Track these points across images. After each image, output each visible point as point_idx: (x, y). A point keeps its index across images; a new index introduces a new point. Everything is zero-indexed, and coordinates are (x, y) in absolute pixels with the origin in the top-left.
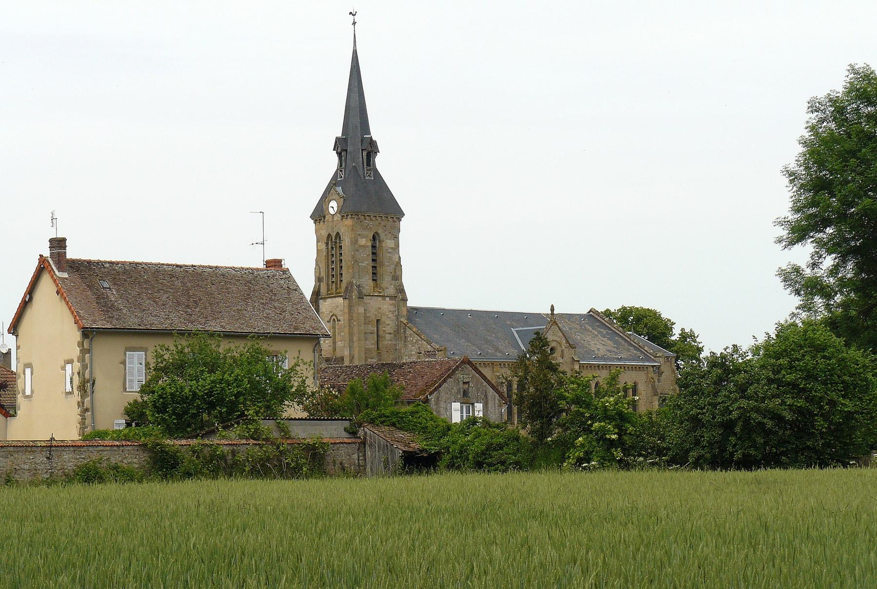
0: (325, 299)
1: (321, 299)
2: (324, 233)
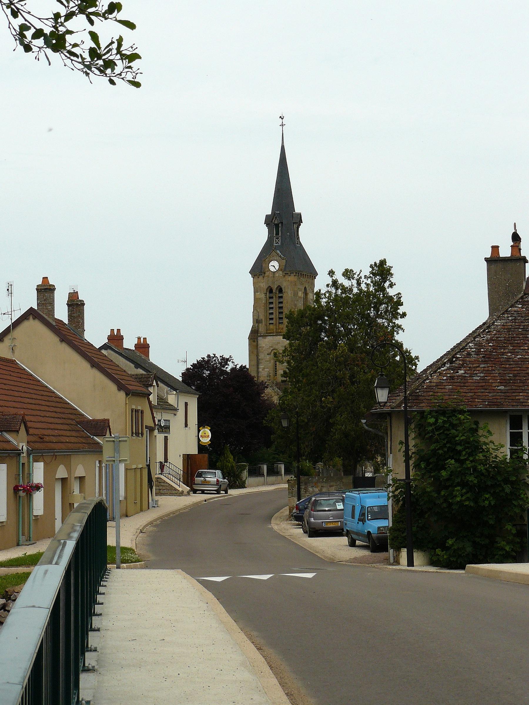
0: (264, 336)
1: (261, 336)
2: (264, 285)
